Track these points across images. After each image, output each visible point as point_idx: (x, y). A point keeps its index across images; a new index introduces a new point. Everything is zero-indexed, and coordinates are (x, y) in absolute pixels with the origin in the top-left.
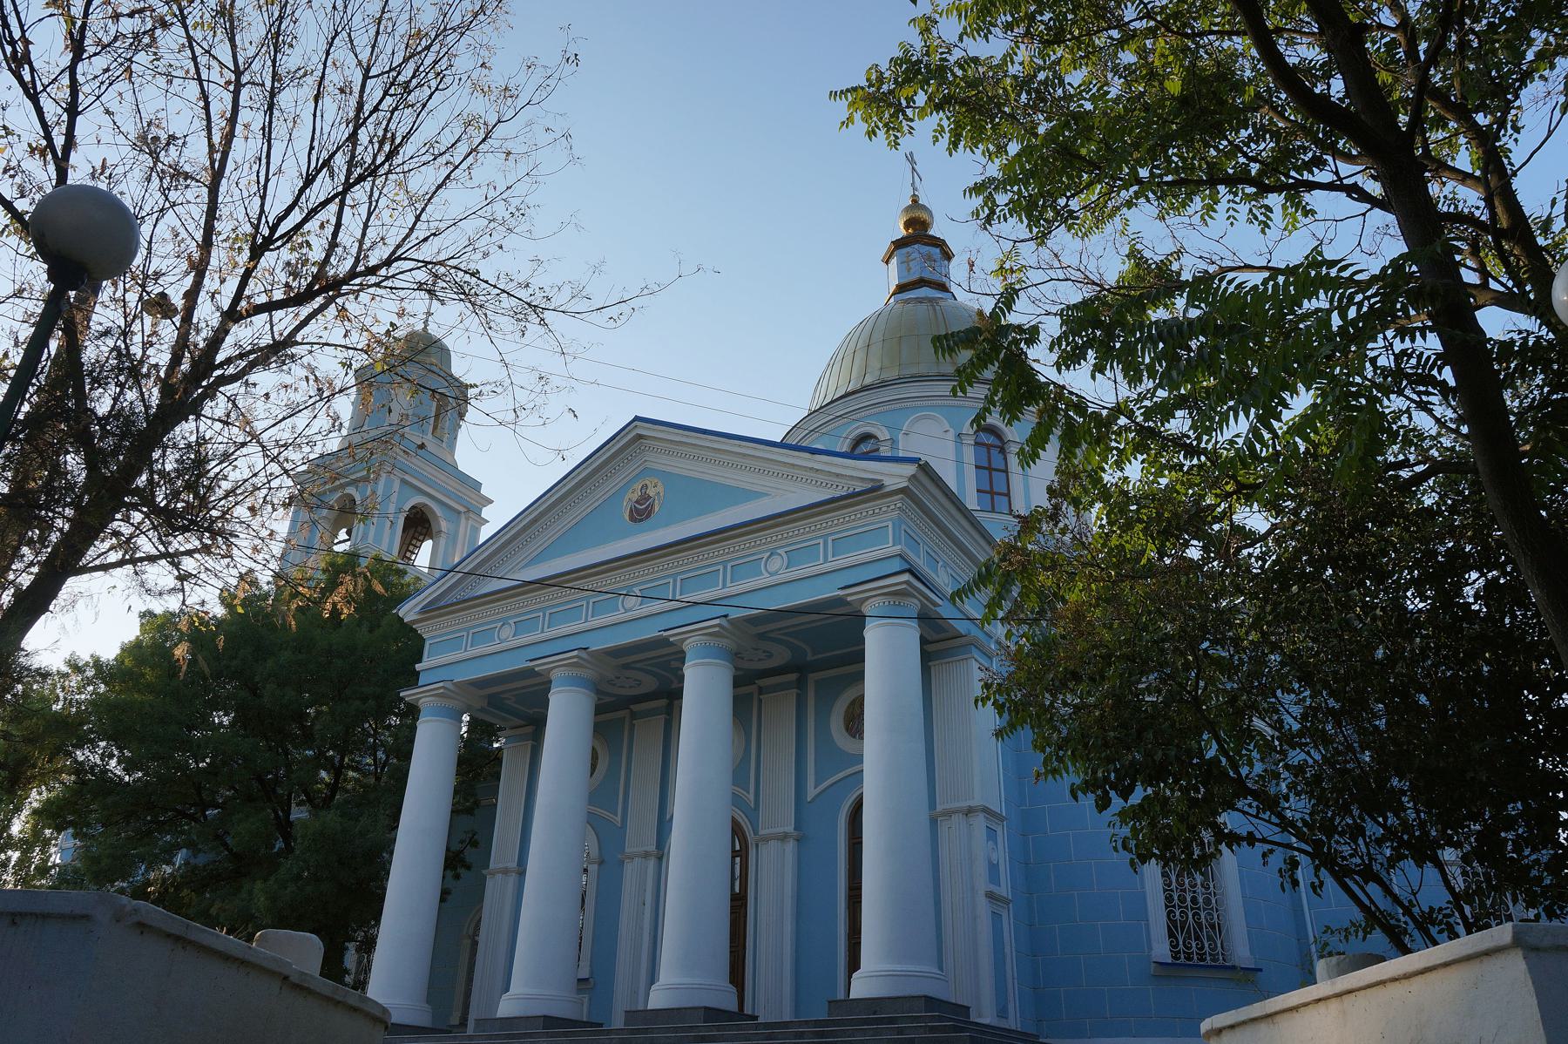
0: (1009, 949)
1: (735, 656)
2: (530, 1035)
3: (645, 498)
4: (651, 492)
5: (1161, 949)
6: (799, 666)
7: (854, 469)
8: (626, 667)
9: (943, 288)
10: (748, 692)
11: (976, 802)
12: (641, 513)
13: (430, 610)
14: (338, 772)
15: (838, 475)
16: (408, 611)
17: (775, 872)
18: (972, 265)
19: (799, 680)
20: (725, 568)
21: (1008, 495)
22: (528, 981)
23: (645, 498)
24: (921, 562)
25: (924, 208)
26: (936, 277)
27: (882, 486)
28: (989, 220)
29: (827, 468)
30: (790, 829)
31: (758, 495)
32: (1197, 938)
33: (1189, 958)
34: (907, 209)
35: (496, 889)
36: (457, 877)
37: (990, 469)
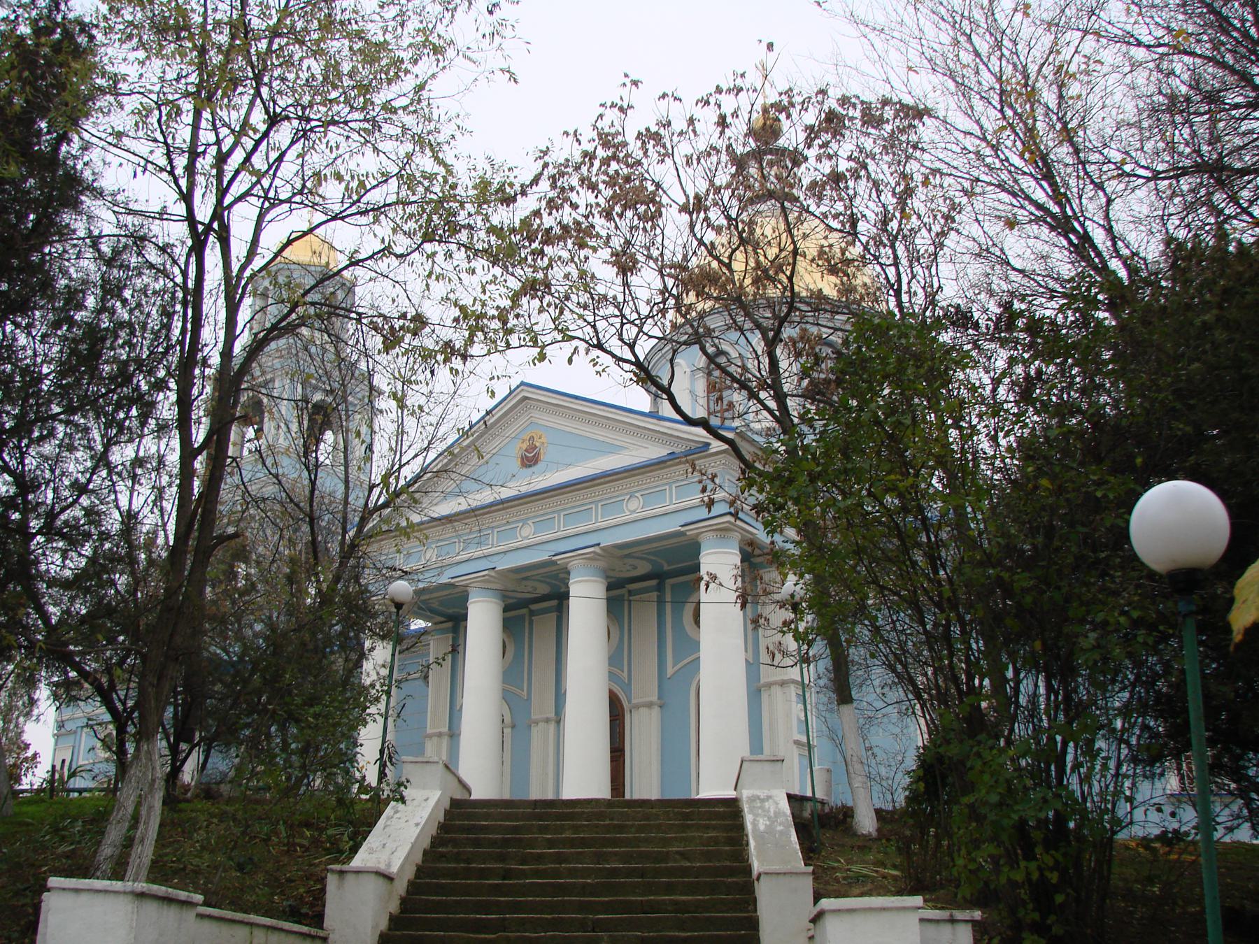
8: (525, 579)
12: (530, 460)
19: (659, 584)
20: (671, 489)
29: (669, 432)
30: (655, 698)
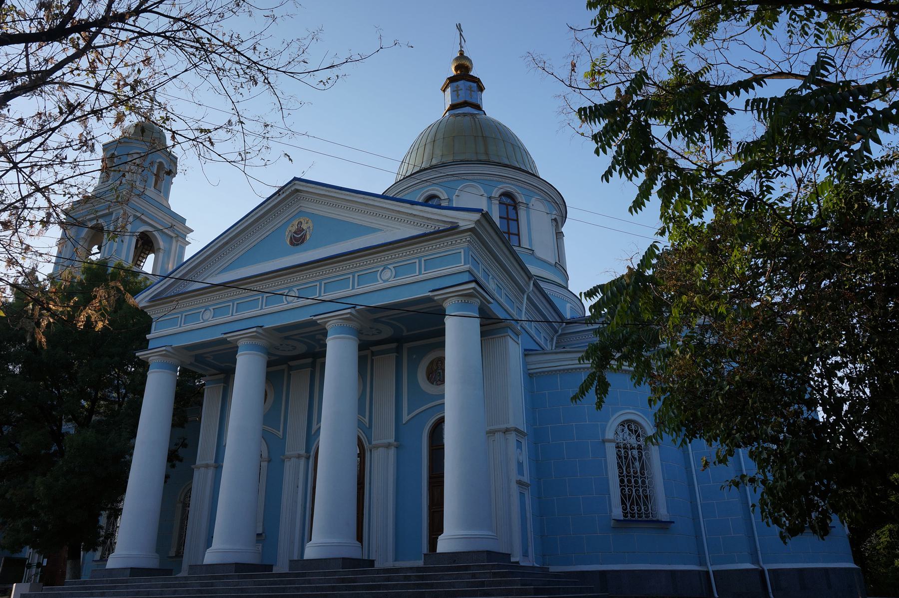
0: (529, 515)
1: (359, 333)
2: (227, 577)
3: (300, 230)
4: (304, 226)
5: (617, 512)
6: (402, 339)
7: (439, 215)
8: (286, 338)
9: (478, 107)
10: (368, 353)
11: (511, 425)
12: (298, 240)
13: (156, 300)
14: (94, 401)
15: (428, 219)
16: (141, 301)
17: (383, 468)
18: (574, 66)
20: (354, 277)
21: (518, 235)
22: (224, 541)
23: (300, 230)
24: (480, 276)
25: (467, 58)
26: (473, 101)
27: (458, 227)
28: (599, 30)
29: (422, 214)
30: (392, 440)
31: (374, 230)
32: (638, 504)
33: (633, 516)
34: (457, 59)
35: (200, 480)
36: (173, 466)
37: (508, 219)
